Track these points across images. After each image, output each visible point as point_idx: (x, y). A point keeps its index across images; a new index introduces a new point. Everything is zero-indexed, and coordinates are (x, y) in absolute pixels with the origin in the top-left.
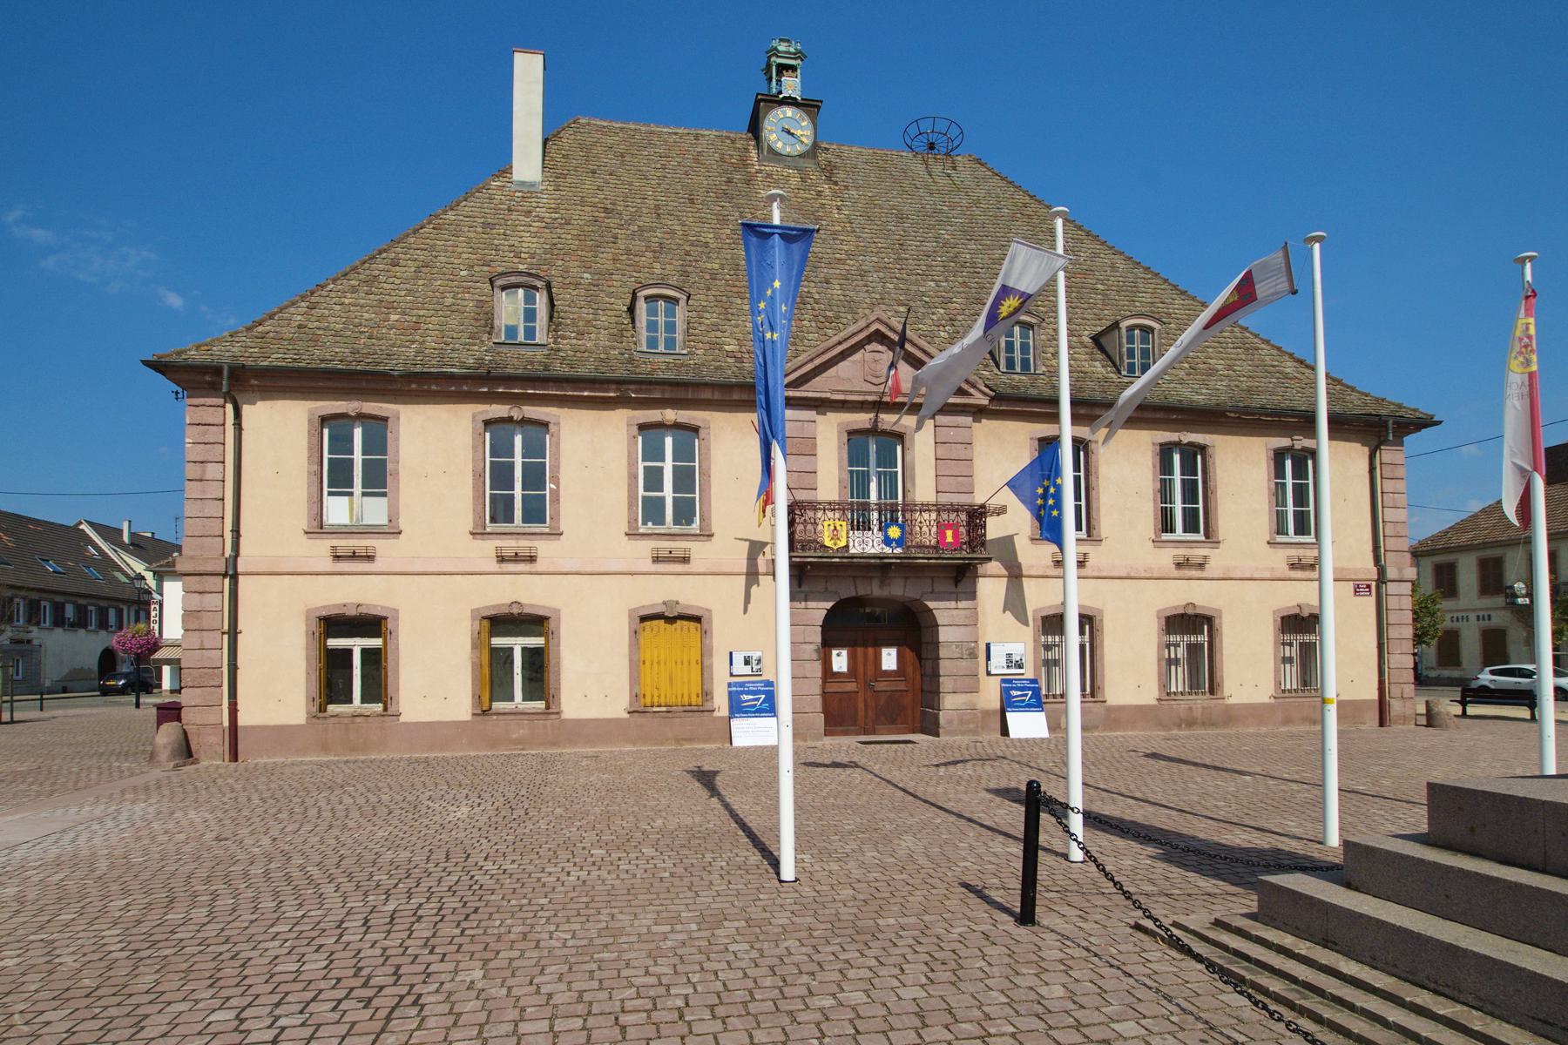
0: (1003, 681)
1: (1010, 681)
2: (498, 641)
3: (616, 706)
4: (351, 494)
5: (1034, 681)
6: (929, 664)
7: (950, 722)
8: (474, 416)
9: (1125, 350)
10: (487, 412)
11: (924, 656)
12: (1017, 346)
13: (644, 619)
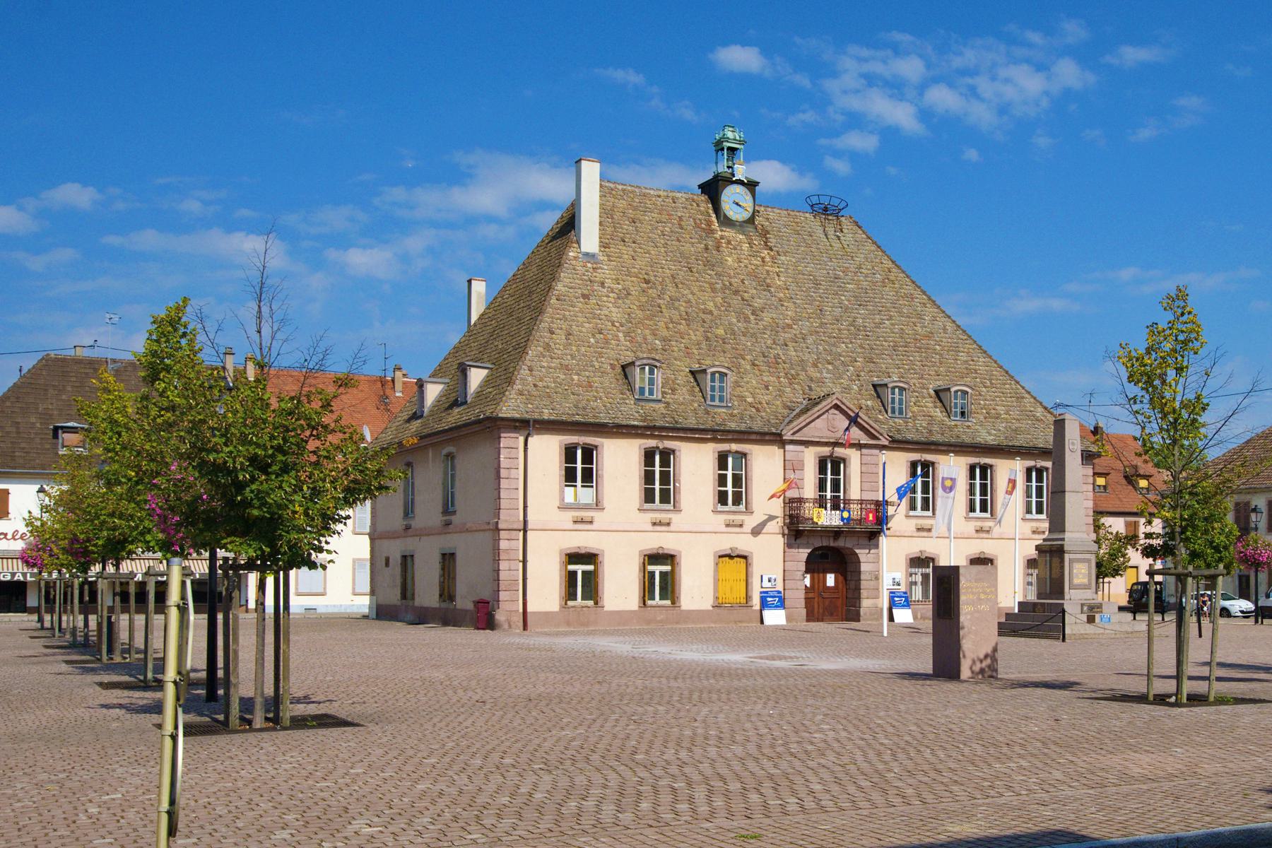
0: (891, 593)
1: (894, 593)
2: (572, 567)
3: (706, 604)
4: (576, 486)
5: (905, 593)
6: (852, 584)
7: (865, 614)
9: (953, 404)
10: (646, 444)
11: (849, 578)
12: (897, 400)
13: (721, 557)
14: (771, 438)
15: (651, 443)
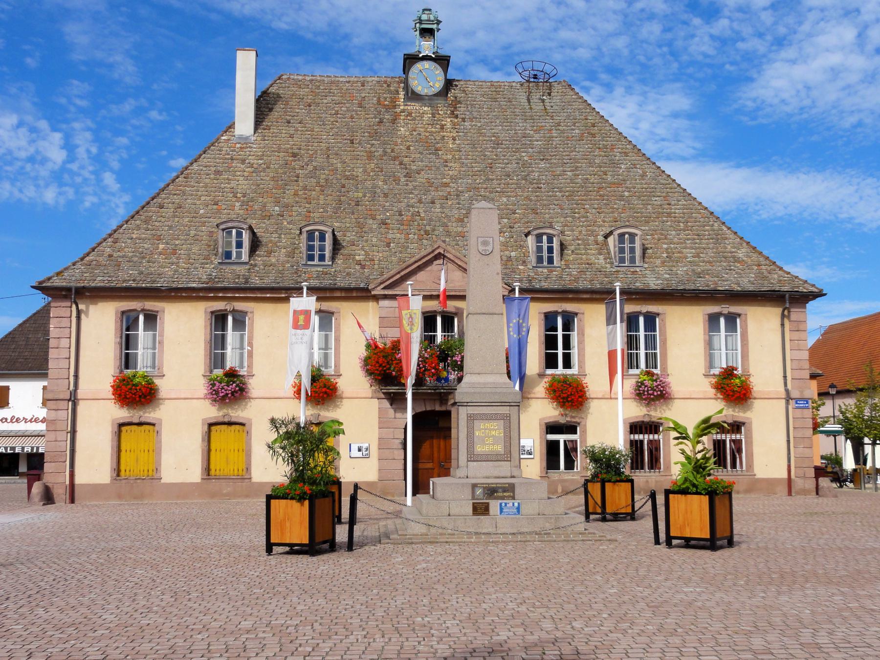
2: (552, 437)
8: (206, 309)
10: (212, 306)
14: (359, 294)
15: (219, 305)
